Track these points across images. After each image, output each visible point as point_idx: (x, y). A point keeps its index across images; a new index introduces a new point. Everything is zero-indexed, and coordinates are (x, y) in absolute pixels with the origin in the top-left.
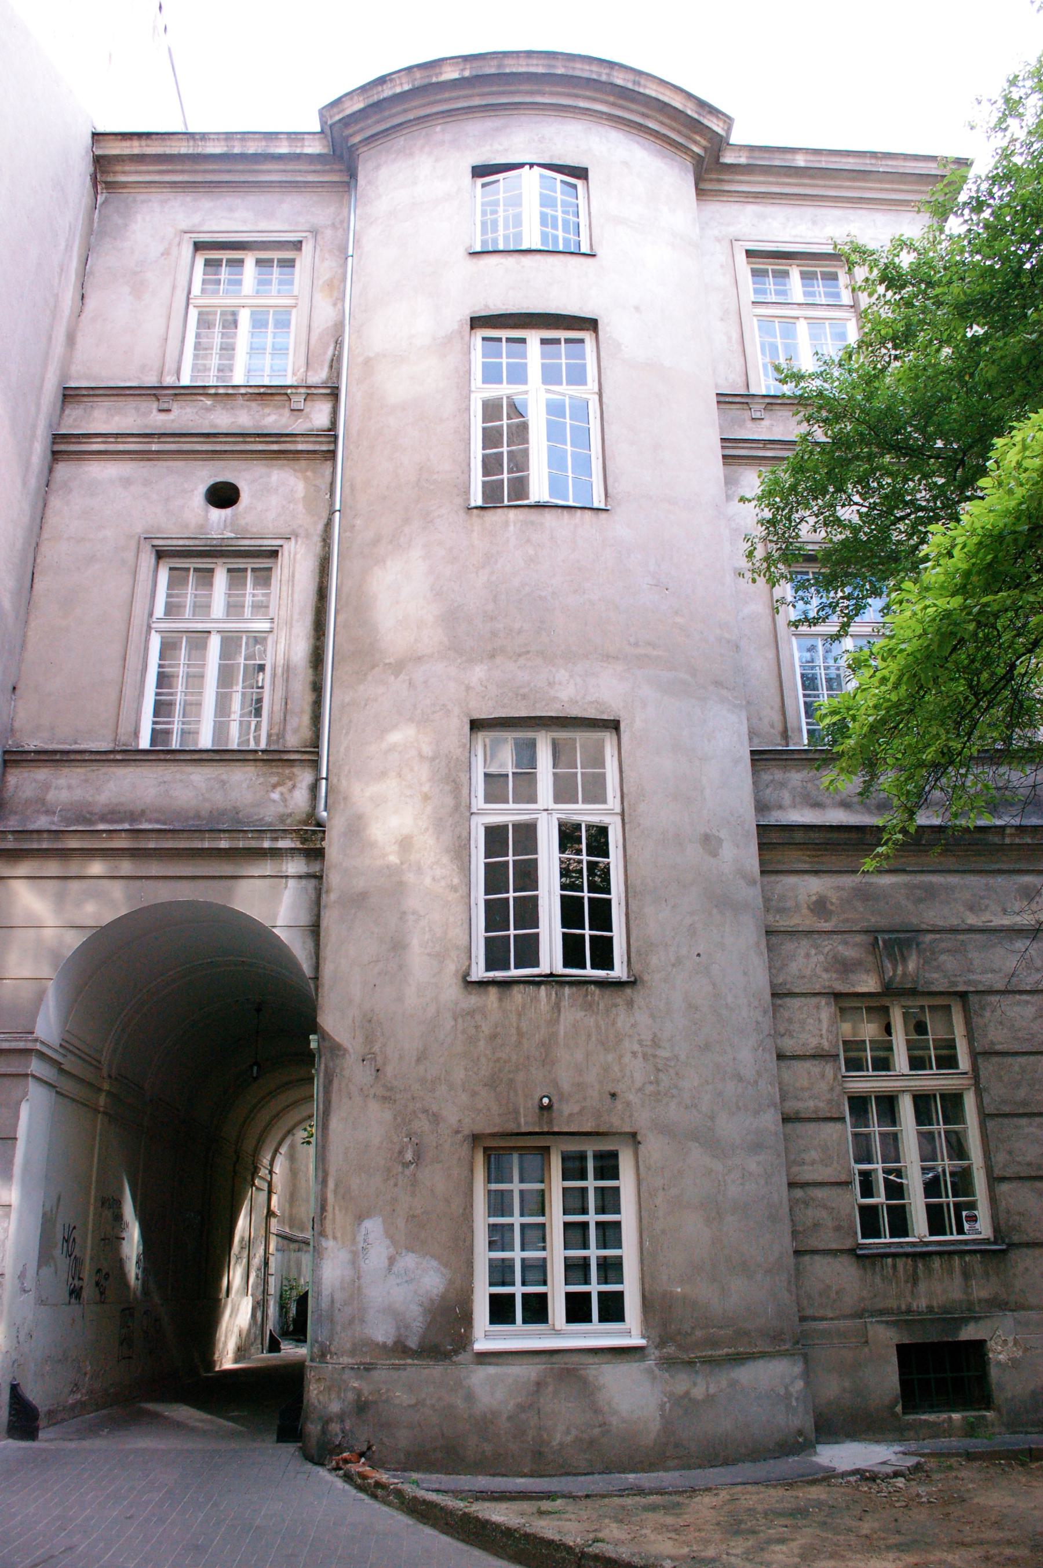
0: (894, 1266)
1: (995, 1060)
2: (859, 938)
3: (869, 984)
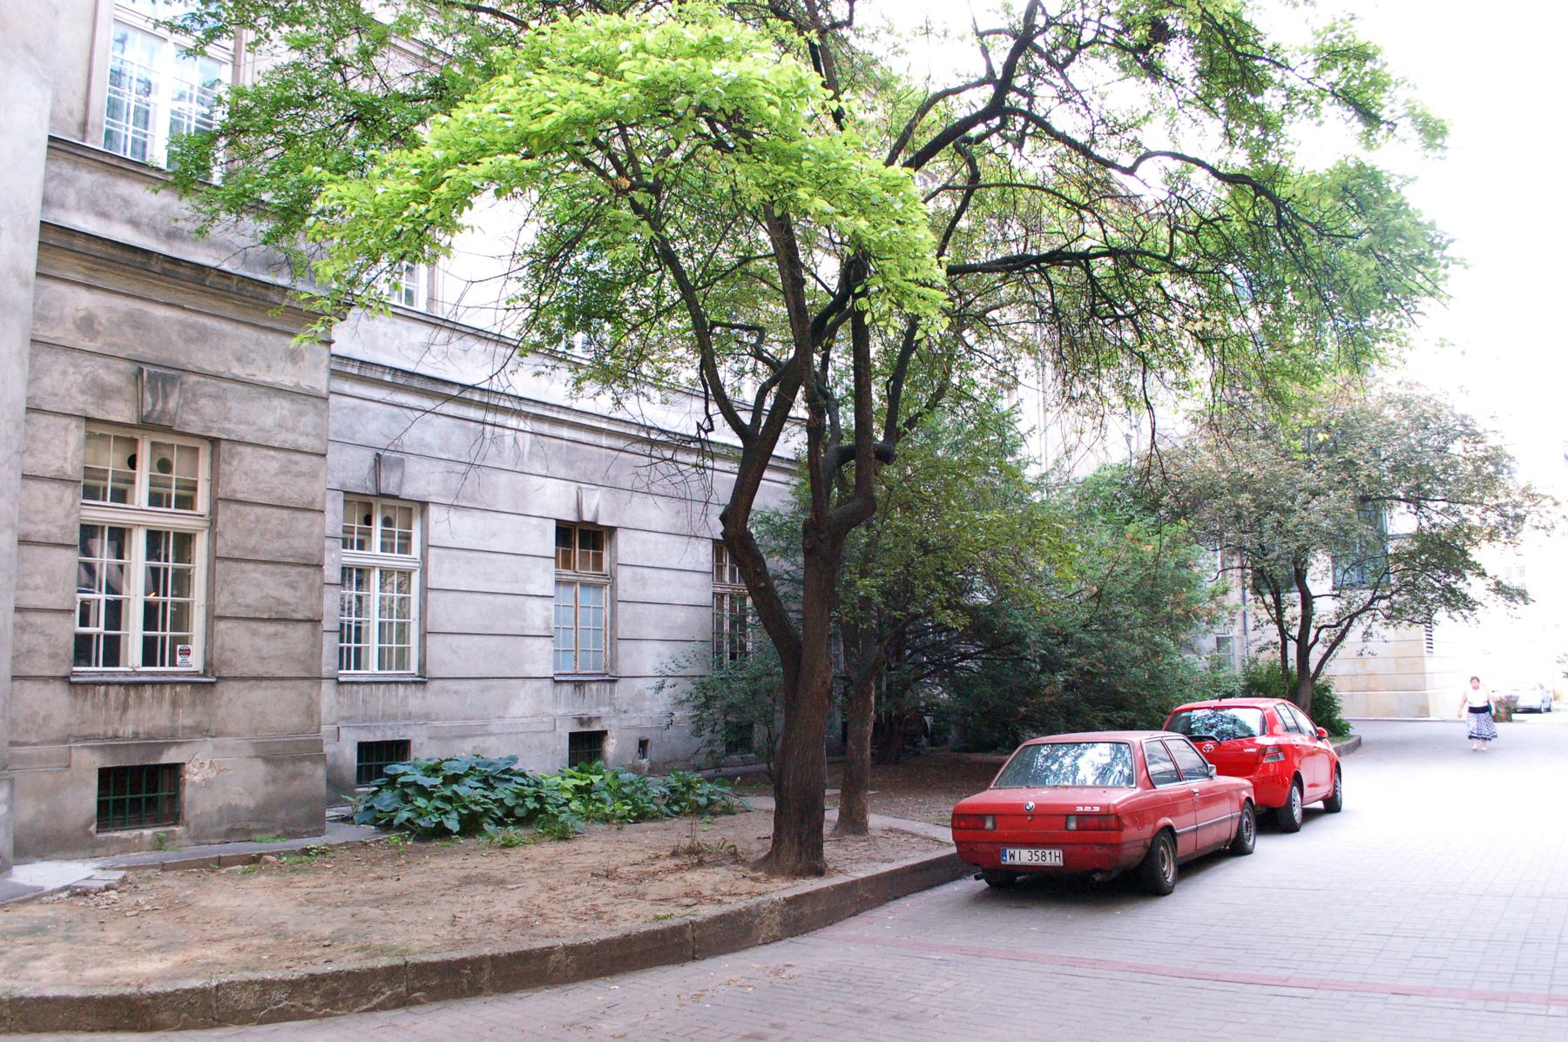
0: (106, 694)
1: (235, 507)
2: (123, 365)
3: (122, 412)
